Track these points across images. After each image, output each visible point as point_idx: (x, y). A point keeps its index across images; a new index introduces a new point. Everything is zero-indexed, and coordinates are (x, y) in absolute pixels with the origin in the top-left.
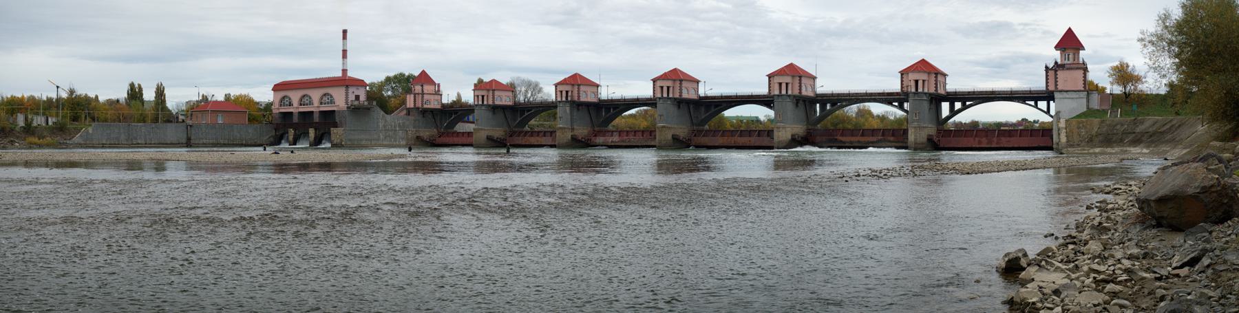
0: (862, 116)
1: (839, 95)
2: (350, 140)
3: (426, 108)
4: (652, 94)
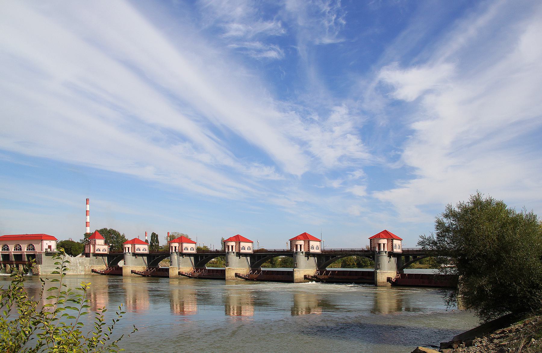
0: (120, 269)
1: (335, 251)
2: (45, 272)
3: (97, 254)
4: (289, 248)
